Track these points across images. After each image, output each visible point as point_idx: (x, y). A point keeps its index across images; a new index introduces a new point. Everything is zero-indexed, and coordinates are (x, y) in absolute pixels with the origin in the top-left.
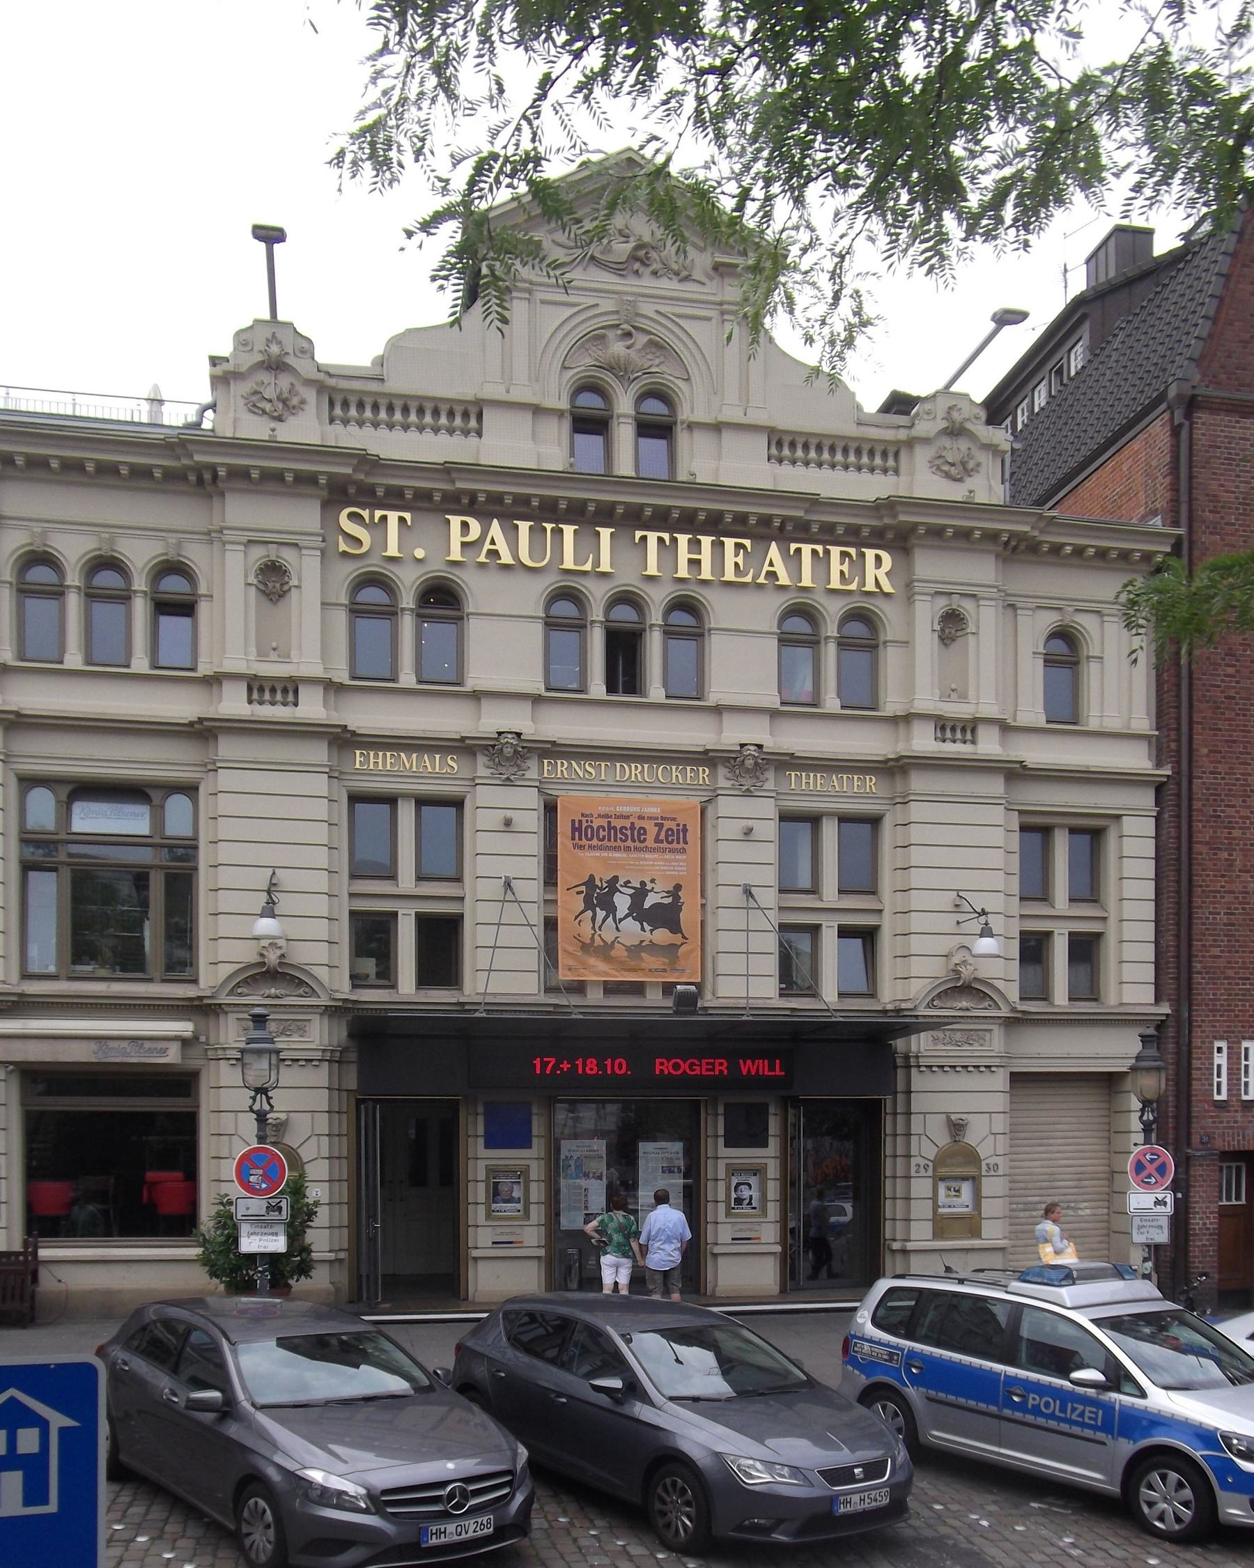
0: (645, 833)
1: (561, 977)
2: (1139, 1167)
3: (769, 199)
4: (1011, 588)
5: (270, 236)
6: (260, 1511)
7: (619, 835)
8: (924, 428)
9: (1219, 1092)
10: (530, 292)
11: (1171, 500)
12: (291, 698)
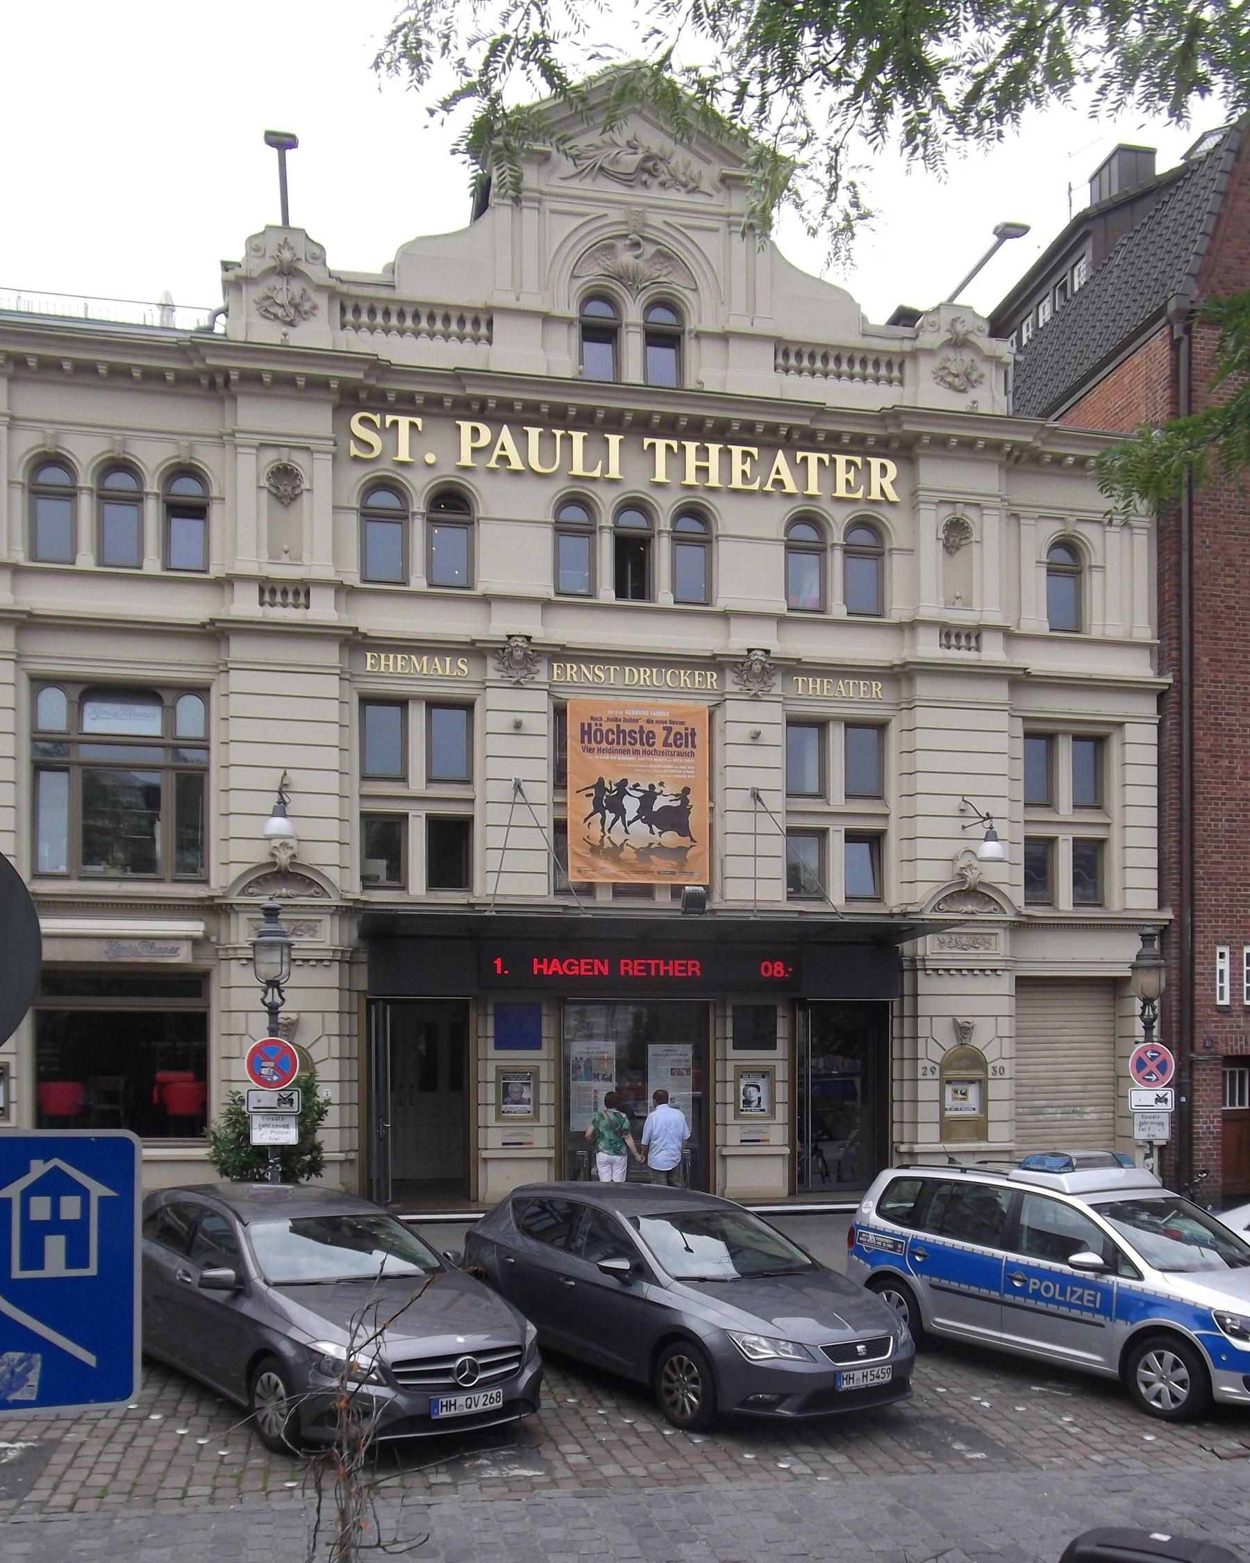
0: (654, 737)
1: (570, 879)
2: (1140, 1064)
3: (764, 96)
4: (1015, 497)
5: (282, 142)
6: (273, 1384)
7: (628, 739)
8: (929, 339)
9: (1222, 998)
10: (540, 201)
11: (1171, 413)
12: (302, 600)
